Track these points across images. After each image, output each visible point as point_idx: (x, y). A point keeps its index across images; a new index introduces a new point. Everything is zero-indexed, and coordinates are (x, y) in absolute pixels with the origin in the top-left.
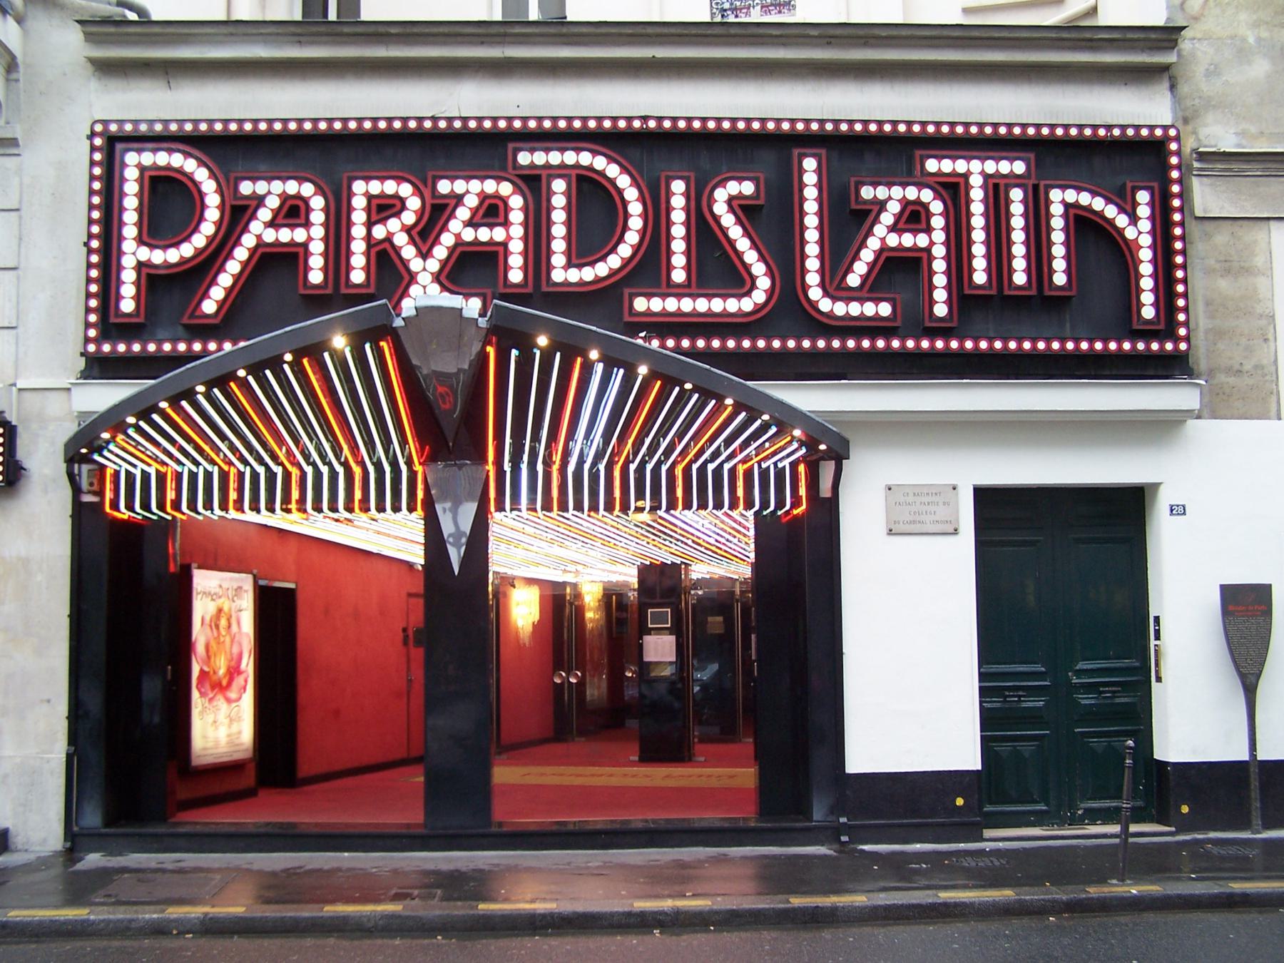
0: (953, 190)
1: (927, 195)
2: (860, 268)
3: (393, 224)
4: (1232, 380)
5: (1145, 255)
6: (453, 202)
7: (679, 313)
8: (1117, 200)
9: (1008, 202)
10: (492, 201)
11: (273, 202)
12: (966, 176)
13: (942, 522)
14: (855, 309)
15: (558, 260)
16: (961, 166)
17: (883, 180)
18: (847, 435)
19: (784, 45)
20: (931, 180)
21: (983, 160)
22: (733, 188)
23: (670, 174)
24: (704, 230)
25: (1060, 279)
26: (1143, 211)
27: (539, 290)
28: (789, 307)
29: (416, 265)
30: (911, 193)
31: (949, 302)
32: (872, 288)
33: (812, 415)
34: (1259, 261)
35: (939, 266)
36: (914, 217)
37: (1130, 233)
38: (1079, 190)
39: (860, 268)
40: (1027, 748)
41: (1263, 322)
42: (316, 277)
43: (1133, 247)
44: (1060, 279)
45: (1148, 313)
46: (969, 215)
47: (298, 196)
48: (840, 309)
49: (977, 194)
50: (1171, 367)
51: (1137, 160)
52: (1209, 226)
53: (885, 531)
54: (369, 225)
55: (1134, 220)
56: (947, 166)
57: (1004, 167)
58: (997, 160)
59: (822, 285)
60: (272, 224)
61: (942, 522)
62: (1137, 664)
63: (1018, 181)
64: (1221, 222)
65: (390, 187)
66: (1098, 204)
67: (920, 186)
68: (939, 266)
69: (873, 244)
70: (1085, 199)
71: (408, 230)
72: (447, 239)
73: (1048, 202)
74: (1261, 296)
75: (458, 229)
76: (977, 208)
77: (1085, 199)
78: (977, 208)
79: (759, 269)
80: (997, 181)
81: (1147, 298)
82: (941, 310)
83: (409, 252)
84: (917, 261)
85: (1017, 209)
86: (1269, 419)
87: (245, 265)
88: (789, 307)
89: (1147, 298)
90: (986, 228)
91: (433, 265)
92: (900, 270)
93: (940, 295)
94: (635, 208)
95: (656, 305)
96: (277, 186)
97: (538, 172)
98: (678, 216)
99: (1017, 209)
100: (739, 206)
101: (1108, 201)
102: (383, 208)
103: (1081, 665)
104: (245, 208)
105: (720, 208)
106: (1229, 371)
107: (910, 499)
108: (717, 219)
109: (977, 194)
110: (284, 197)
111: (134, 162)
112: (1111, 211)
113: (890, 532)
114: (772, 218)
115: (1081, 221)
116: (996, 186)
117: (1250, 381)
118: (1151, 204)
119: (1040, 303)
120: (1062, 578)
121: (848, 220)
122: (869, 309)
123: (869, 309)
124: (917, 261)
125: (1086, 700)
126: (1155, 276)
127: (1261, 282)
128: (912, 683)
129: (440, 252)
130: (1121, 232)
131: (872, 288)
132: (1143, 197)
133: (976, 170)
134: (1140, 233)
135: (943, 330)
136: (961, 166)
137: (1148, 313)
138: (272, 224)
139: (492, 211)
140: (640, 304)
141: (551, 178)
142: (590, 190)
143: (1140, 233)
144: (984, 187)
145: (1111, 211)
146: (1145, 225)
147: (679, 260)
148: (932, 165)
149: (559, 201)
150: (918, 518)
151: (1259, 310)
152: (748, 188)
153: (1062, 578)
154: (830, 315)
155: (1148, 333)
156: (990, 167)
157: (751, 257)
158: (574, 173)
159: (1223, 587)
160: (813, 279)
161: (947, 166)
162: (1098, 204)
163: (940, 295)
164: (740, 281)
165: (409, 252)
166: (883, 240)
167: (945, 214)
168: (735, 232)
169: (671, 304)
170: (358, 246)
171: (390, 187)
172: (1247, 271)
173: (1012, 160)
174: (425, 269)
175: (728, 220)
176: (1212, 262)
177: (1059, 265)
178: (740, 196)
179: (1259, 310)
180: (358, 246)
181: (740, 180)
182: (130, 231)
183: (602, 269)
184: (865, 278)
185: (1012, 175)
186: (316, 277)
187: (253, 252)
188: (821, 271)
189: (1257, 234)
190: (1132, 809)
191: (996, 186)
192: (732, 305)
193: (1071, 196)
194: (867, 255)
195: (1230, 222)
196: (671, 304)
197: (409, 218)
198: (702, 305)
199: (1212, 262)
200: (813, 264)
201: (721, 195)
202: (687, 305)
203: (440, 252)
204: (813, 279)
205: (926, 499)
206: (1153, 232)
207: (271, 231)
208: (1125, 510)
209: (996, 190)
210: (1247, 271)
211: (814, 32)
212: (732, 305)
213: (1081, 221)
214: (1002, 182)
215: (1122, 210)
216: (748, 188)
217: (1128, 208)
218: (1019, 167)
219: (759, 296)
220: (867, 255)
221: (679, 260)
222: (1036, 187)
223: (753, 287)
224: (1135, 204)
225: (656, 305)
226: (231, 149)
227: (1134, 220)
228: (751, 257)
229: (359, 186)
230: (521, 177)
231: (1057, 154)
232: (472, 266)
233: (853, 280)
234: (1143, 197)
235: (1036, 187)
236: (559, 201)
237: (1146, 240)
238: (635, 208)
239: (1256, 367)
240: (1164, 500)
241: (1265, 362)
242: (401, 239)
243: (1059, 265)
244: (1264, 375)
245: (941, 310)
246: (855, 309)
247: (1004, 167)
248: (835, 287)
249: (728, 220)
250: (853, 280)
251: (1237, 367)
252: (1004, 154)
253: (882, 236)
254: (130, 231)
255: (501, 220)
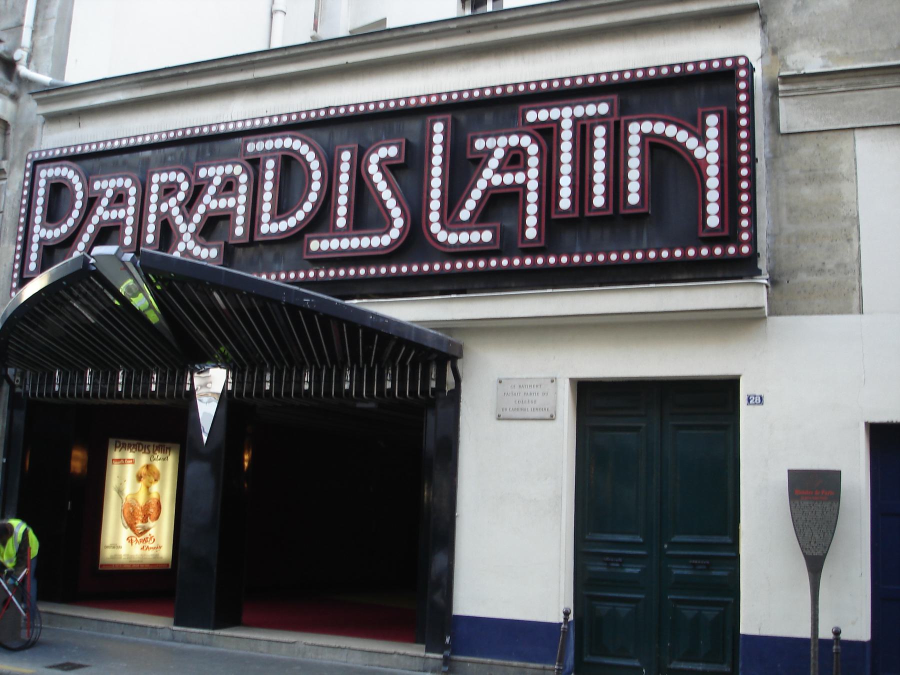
0: (547, 134)
1: (526, 141)
2: (471, 205)
3: (172, 201)
4: (815, 279)
5: (713, 171)
6: (485, 156)
7: (340, 250)
8: (689, 126)
9: (593, 138)
10: (516, 152)
11: (499, 154)
12: (558, 122)
13: (541, 409)
14: (464, 238)
15: (266, 218)
16: (555, 114)
17: (503, 131)
18: (455, 338)
19: (436, 39)
20: (530, 129)
21: (573, 106)
22: (383, 152)
23: (341, 147)
24: (361, 185)
25: (634, 199)
26: (712, 133)
27: (253, 240)
28: (415, 240)
29: (182, 228)
30: (514, 140)
31: (538, 227)
32: (481, 218)
33: (415, 325)
34: (844, 168)
35: (532, 197)
36: (515, 159)
37: (699, 153)
38: (654, 121)
39: (471, 205)
40: (624, 610)
41: (847, 224)
42: (239, 231)
43: (702, 167)
44: (634, 199)
45: (713, 221)
46: (559, 152)
47: (519, 147)
48: (453, 239)
49: (567, 135)
50: (742, 268)
51: (713, 88)
52: (793, 141)
53: (494, 416)
54: (159, 204)
55: (703, 140)
56: (543, 115)
57: (591, 110)
58: (585, 105)
59: (441, 221)
60: (500, 171)
61: (541, 409)
62: (641, 540)
63: (601, 120)
64: (807, 136)
65: (172, 176)
66: (671, 131)
67: (520, 134)
68: (532, 197)
69: (482, 184)
70: (659, 128)
71: (179, 204)
72: (201, 209)
73: (627, 134)
74: (845, 200)
75: (209, 202)
76: (566, 146)
77: (659, 128)
78: (566, 146)
79: (396, 212)
80: (584, 122)
81: (713, 209)
82: (531, 233)
83: (179, 220)
84: (516, 194)
85: (600, 143)
86: (850, 312)
87: (479, 203)
88: (415, 240)
89: (713, 209)
90: (573, 163)
91: (192, 228)
92: (501, 202)
93: (531, 221)
94: (317, 175)
95: (325, 245)
96: (502, 141)
97: (258, 156)
98: (344, 178)
99: (600, 143)
100: (388, 166)
101: (680, 127)
102: (169, 190)
103: (677, 539)
104: (202, 186)
105: (373, 169)
106: (811, 270)
107: (516, 390)
108: (370, 177)
109: (567, 135)
110: (508, 149)
111: (46, 174)
112: (682, 136)
113: (499, 418)
114: (408, 170)
115: (654, 146)
116: (583, 127)
117: (832, 279)
118: (720, 126)
119: (618, 220)
120: (657, 457)
121: (463, 166)
122: (475, 237)
123: (475, 237)
124: (517, 194)
125: (679, 570)
126: (720, 189)
127: (845, 188)
128: (514, 541)
129: (197, 218)
130: (691, 153)
131: (481, 218)
132: (712, 120)
133: (565, 116)
134: (708, 153)
135: (532, 250)
136: (555, 114)
137: (713, 221)
138: (500, 171)
139: (229, 186)
140: (314, 245)
141: (266, 160)
142: (289, 163)
143: (708, 153)
144: (573, 129)
145: (682, 136)
146: (713, 145)
147: (342, 211)
148: (531, 116)
149: (269, 175)
150: (521, 406)
151: (843, 212)
152: (393, 151)
153: (657, 457)
154: (445, 244)
155: (712, 239)
156: (579, 111)
157: (391, 203)
158: (279, 154)
159: (791, 473)
160: (434, 216)
161: (543, 115)
162: (671, 131)
163: (531, 221)
164: (384, 223)
165: (179, 220)
166: (489, 181)
167: (540, 155)
168: (382, 186)
169: (335, 244)
170: (152, 218)
171: (172, 176)
172: (833, 178)
173: (597, 104)
174: (186, 229)
175: (377, 177)
176: (797, 172)
177: (634, 187)
178: (388, 158)
179: (843, 212)
180: (152, 218)
181: (387, 146)
182: (38, 219)
183: (292, 222)
184: (473, 213)
185: (597, 116)
186: (239, 231)
187: (485, 192)
188: (441, 210)
189: (842, 144)
190: (559, 662)
191: (583, 127)
192: (376, 242)
193: (647, 127)
194: (476, 194)
195: (813, 135)
196: (335, 244)
197: (181, 196)
198: (355, 243)
199: (797, 172)
200: (435, 205)
201: (374, 159)
202: (345, 244)
203: (197, 218)
204: (434, 216)
205: (528, 390)
206: (720, 151)
207: (107, 212)
208: (718, 400)
209: (583, 130)
210: (833, 178)
211: (453, 25)
212: (376, 242)
213: (654, 146)
214: (588, 123)
215: (691, 134)
216: (393, 151)
217: (698, 131)
218: (604, 108)
219: (395, 233)
220: (476, 194)
221: (342, 211)
222: (617, 124)
223: (391, 226)
224: (705, 127)
225: (325, 245)
226: (91, 161)
227: (703, 140)
228: (391, 203)
229: (634, 128)
230: (249, 161)
231: (633, 94)
232: (212, 227)
233: (464, 215)
234: (712, 120)
235: (617, 124)
236: (269, 175)
237: (713, 158)
238: (317, 175)
239: (838, 266)
240: (744, 391)
241: (848, 260)
242: (176, 211)
243: (634, 187)
244: (846, 273)
245: (531, 233)
246: (464, 238)
247: (591, 110)
248: (449, 220)
249: (377, 177)
250: (464, 215)
251: (818, 266)
252: (543, 105)
253: (490, 176)
254: (38, 219)
255: (522, 166)
